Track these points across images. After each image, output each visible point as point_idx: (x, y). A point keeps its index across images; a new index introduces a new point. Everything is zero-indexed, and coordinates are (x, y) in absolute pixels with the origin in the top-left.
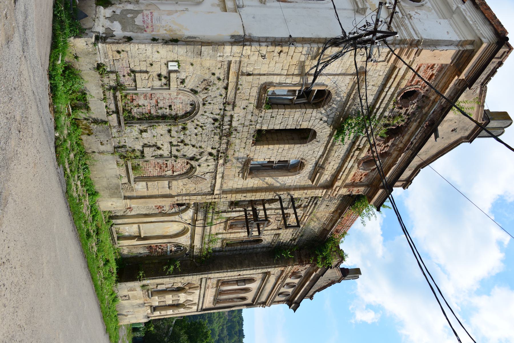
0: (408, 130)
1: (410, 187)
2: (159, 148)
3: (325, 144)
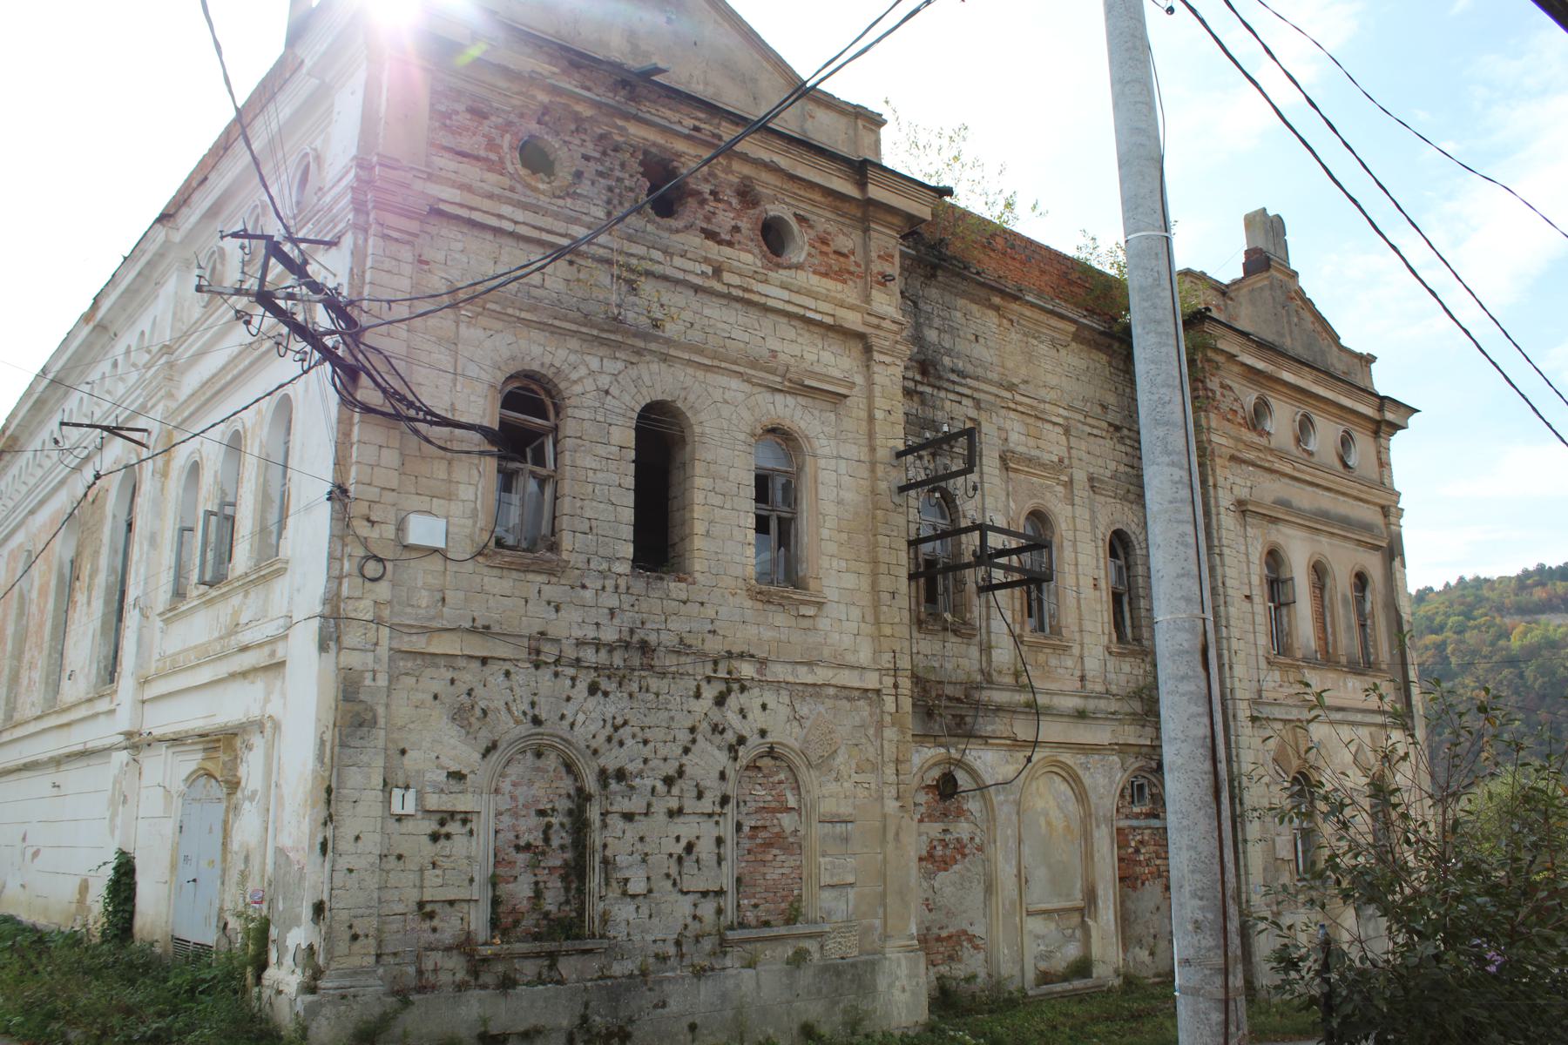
0: (654, 144)
2: (689, 848)
3: (700, 374)
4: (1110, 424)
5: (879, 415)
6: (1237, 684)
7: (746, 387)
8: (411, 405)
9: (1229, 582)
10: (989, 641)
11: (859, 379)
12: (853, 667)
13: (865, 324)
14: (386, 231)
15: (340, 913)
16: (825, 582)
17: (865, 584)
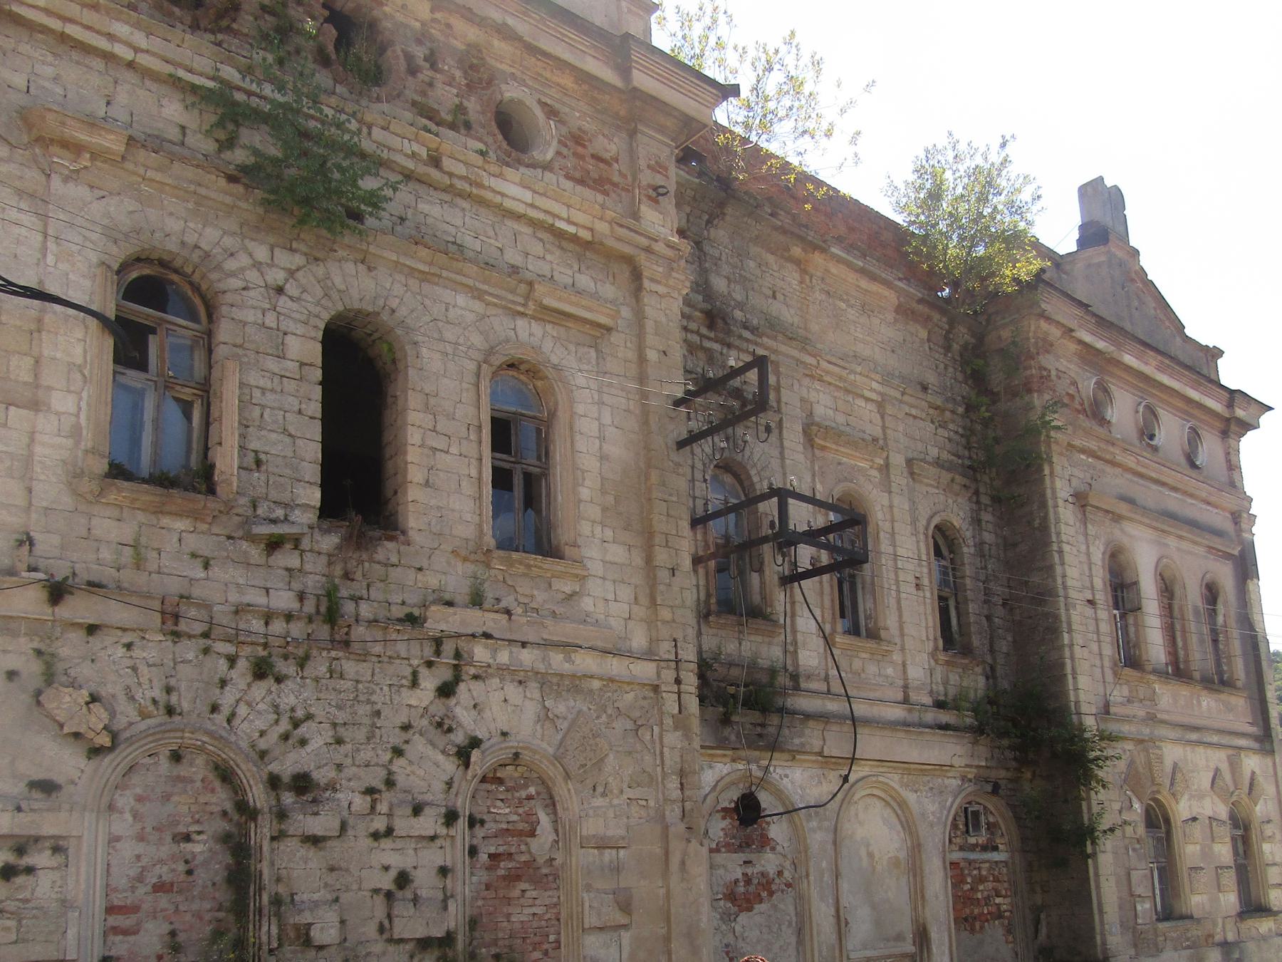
5: (652, 355)
6: (1082, 697)
9: (1070, 583)
11: (626, 312)
17: (638, 560)
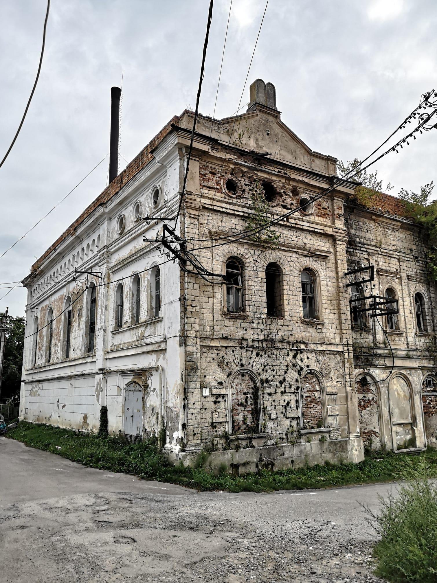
0: (266, 178)
1: (333, 156)
2: (288, 403)
3: (283, 253)
4: (414, 256)
5: (339, 261)
7: (297, 256)
8: (203, 270)
10: (375, 332)
11: (332, 250)
12: (334, 344)
13: (333, 232)
14: (190, 215)
15: (190, 426)
16: (324, 317)
17: (336, 316)
